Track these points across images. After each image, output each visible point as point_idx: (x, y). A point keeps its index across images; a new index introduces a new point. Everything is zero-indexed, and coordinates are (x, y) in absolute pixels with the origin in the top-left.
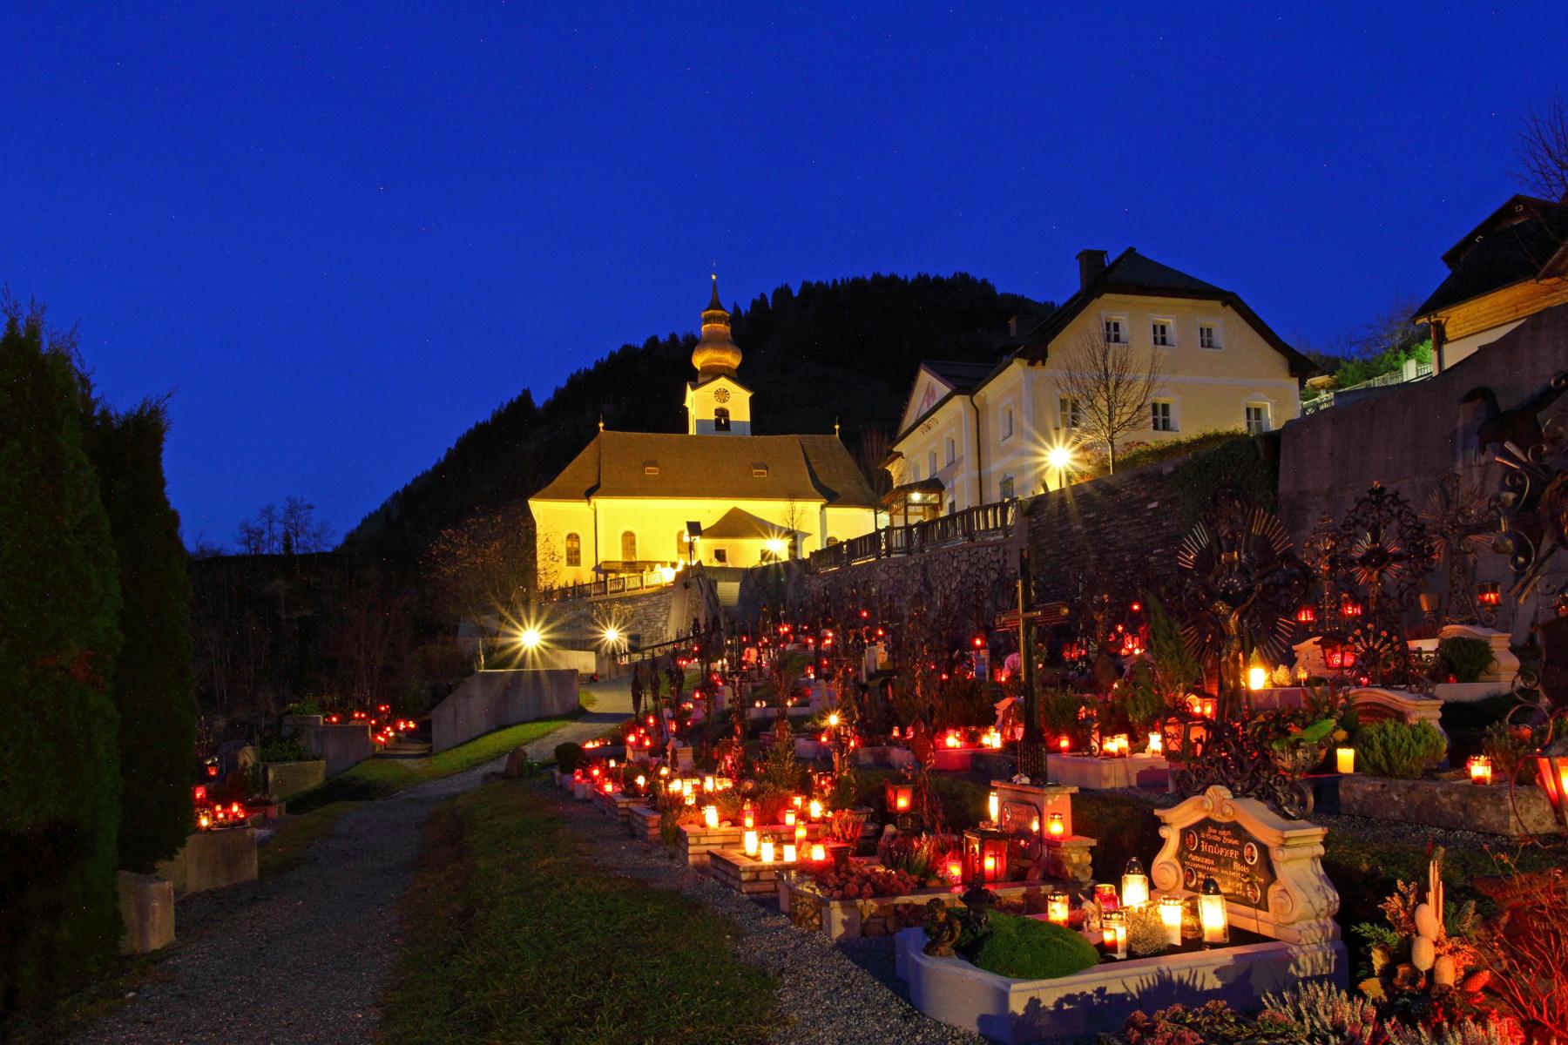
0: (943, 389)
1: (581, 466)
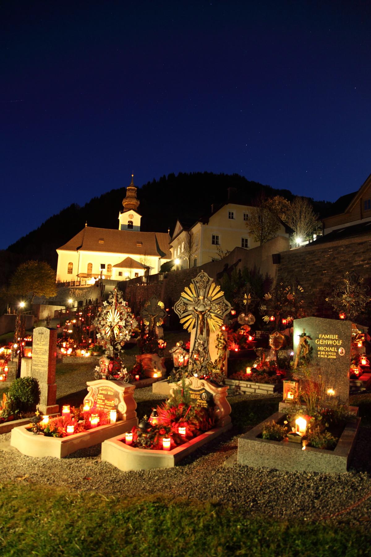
1: (76, 239)
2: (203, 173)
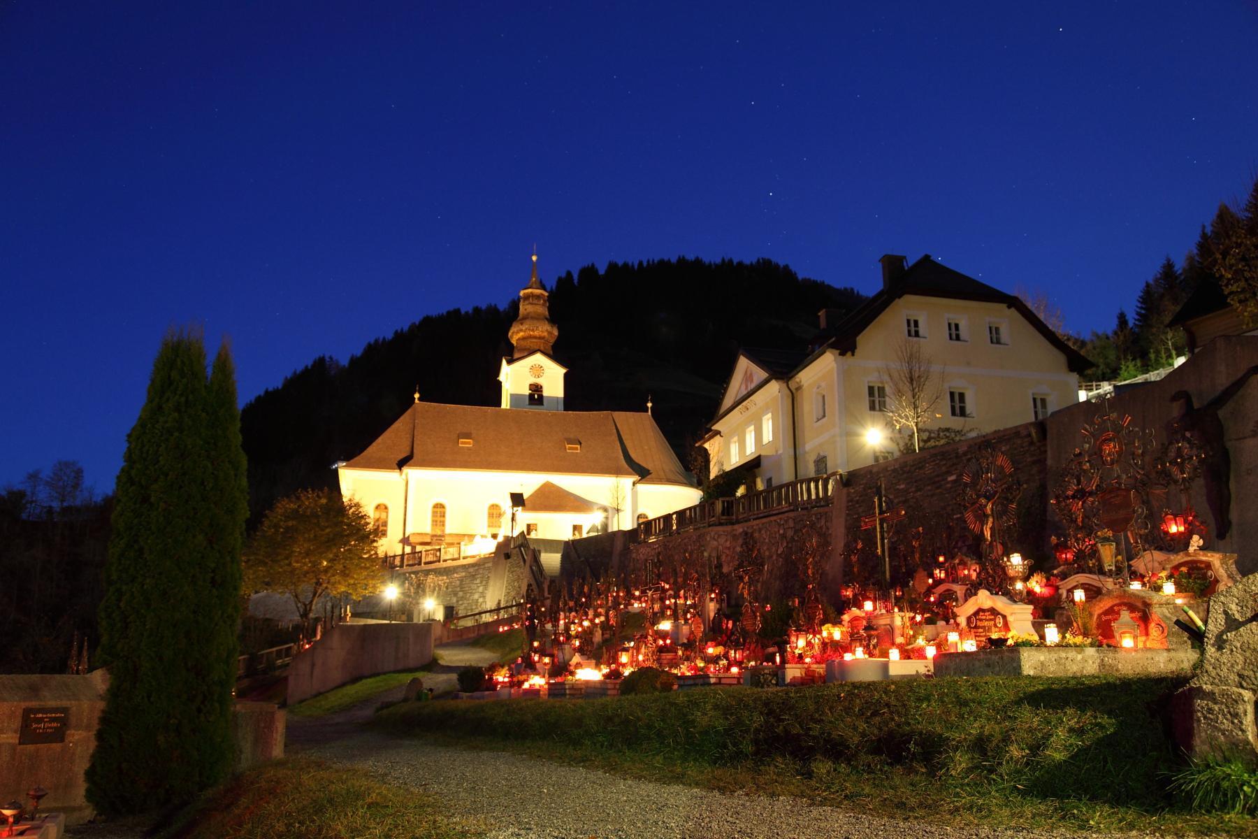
0: (760, 374)
1: (393, 437)
2: (674, 260)
